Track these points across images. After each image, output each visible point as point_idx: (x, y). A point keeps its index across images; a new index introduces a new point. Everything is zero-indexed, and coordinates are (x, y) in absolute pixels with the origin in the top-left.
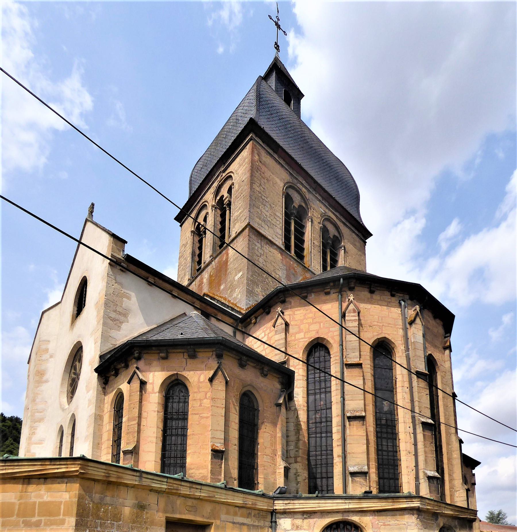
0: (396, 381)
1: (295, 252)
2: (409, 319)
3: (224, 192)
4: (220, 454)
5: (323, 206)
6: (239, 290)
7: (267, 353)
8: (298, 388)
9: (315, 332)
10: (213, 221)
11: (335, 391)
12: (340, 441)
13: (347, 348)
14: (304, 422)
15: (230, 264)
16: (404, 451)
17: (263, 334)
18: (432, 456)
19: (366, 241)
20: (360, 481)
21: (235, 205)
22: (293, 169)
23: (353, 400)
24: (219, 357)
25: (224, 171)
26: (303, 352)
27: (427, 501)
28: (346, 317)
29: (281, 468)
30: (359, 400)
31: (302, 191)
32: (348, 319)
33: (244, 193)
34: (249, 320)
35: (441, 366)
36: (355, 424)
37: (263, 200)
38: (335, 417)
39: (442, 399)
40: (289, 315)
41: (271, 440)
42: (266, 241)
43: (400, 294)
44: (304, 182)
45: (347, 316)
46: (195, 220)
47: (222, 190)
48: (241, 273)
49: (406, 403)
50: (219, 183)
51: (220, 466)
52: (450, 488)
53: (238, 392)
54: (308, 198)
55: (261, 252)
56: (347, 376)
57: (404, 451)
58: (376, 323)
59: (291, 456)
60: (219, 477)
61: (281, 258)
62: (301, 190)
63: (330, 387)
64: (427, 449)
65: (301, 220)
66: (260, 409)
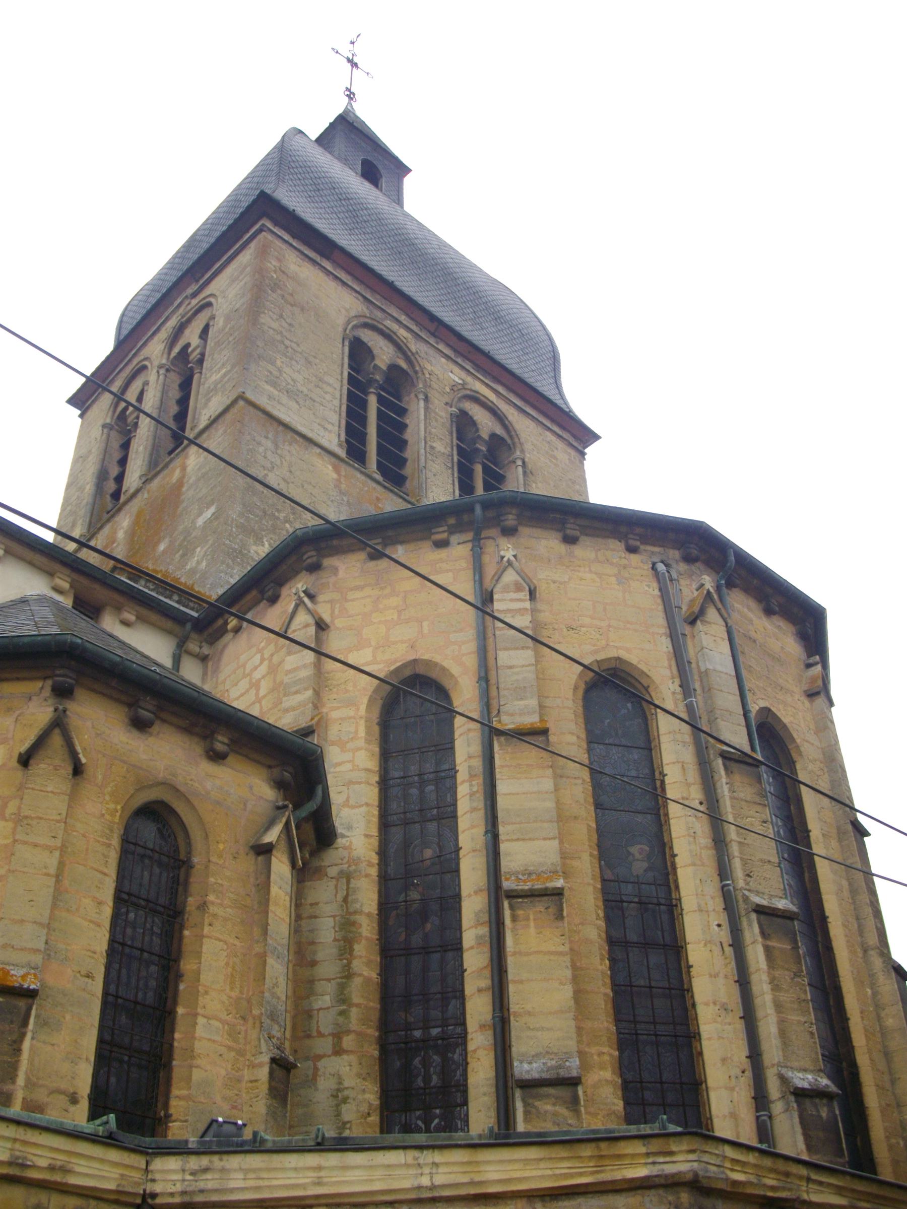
0: (663, 782)
1: (380, 466)
2: (686, 612)
3: (192, 336)
4: (22, 1003)
5: (456, 369)
6: (205, 549)
7: (265, 709)
8: (353, 807)
9: (407, 645)
10: (158, 399)
11: (468, 815)
12: (487, 973)
13: (501, 686)
14: (369, 915)
15: (187, 490)
16: (707, 1004)
17: (258, 656)
18: (803, 1019)
19: (586, 451)
20: (555, 1114)
21: (212, 359)
22: (373, 290)
23: (523, 840)
24: (62, 692)
25: (194, 295)
26: (369, 701)
27: (729, 1152)
28: (495, 603)
29: (261, 1065)
30: (545, 839)
31: (397, 336)
32: (501, 609)
33: (236, 334)
34: (220, 622)
35: (805, 743)
36: (532, 917)
37: (287, 347)
38: (469, 896)
39: (821, 838)
40: (331, 602)
41: (227, 964)
42: (290, 435)
43: (654, 545)
44: (403, 318)
45: (499, 600)
46: (119, 397)
47: (187, 332)
48: (212, 510)
49: (701, 848)
50: (182, 317)
51: (15, 1046)
52: (887, 1137)
53: (117, 803)
54: (414, 351)
55: (273, 460)
56: (502, 767)
57: (707, 1004)
58: (587, 620)
59: (322, 1029)
60: (7, 1087)
61: (335, 476)
62: (395, 333)
63: (455, 804)
64: (784, 997)
65: (399, 398)
66: (195, 860)
